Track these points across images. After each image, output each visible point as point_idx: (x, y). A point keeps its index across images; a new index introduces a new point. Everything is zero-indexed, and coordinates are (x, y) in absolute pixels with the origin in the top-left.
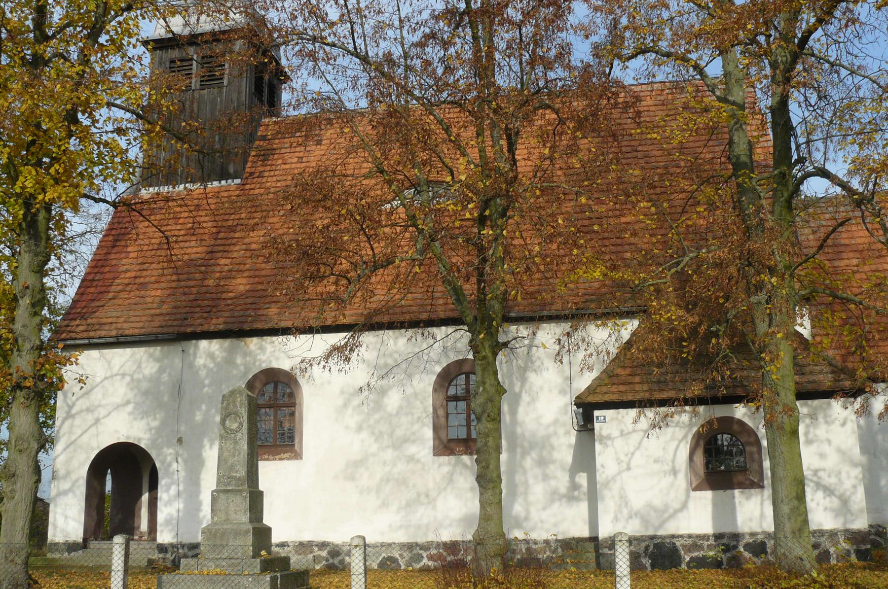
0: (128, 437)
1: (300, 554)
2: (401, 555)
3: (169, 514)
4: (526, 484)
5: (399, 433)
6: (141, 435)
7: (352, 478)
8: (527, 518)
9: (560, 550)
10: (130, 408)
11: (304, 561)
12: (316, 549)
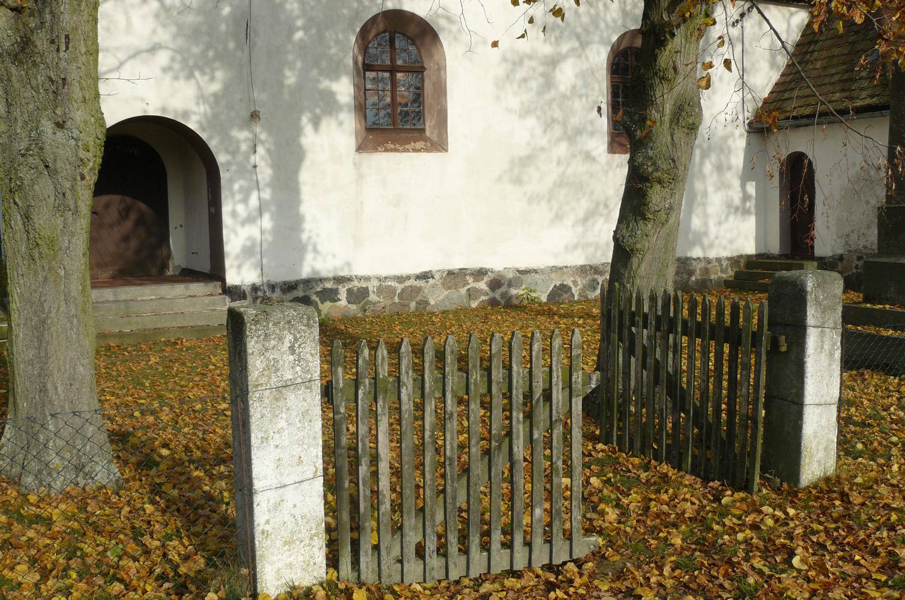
0: (164, 109)
1: (449, 288)
2: (575, 282)
3: (249, 238)
4: (705, 194)
5: (575, 121)
6: (192, 106)
7: (518, 181)
8: (706, 234)
9: (579, 280)
10: (163, 58)
11: (455, 296)
12: (470, 279)
